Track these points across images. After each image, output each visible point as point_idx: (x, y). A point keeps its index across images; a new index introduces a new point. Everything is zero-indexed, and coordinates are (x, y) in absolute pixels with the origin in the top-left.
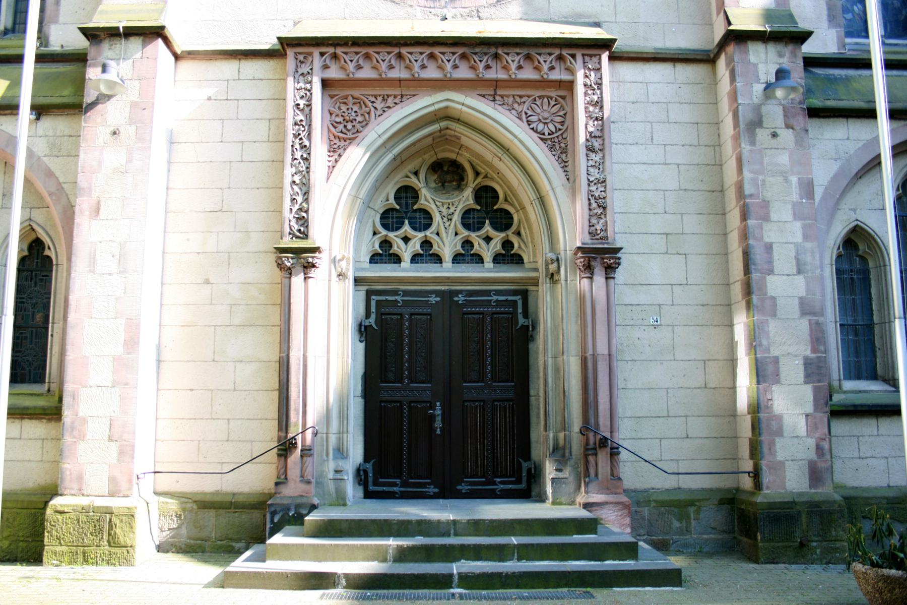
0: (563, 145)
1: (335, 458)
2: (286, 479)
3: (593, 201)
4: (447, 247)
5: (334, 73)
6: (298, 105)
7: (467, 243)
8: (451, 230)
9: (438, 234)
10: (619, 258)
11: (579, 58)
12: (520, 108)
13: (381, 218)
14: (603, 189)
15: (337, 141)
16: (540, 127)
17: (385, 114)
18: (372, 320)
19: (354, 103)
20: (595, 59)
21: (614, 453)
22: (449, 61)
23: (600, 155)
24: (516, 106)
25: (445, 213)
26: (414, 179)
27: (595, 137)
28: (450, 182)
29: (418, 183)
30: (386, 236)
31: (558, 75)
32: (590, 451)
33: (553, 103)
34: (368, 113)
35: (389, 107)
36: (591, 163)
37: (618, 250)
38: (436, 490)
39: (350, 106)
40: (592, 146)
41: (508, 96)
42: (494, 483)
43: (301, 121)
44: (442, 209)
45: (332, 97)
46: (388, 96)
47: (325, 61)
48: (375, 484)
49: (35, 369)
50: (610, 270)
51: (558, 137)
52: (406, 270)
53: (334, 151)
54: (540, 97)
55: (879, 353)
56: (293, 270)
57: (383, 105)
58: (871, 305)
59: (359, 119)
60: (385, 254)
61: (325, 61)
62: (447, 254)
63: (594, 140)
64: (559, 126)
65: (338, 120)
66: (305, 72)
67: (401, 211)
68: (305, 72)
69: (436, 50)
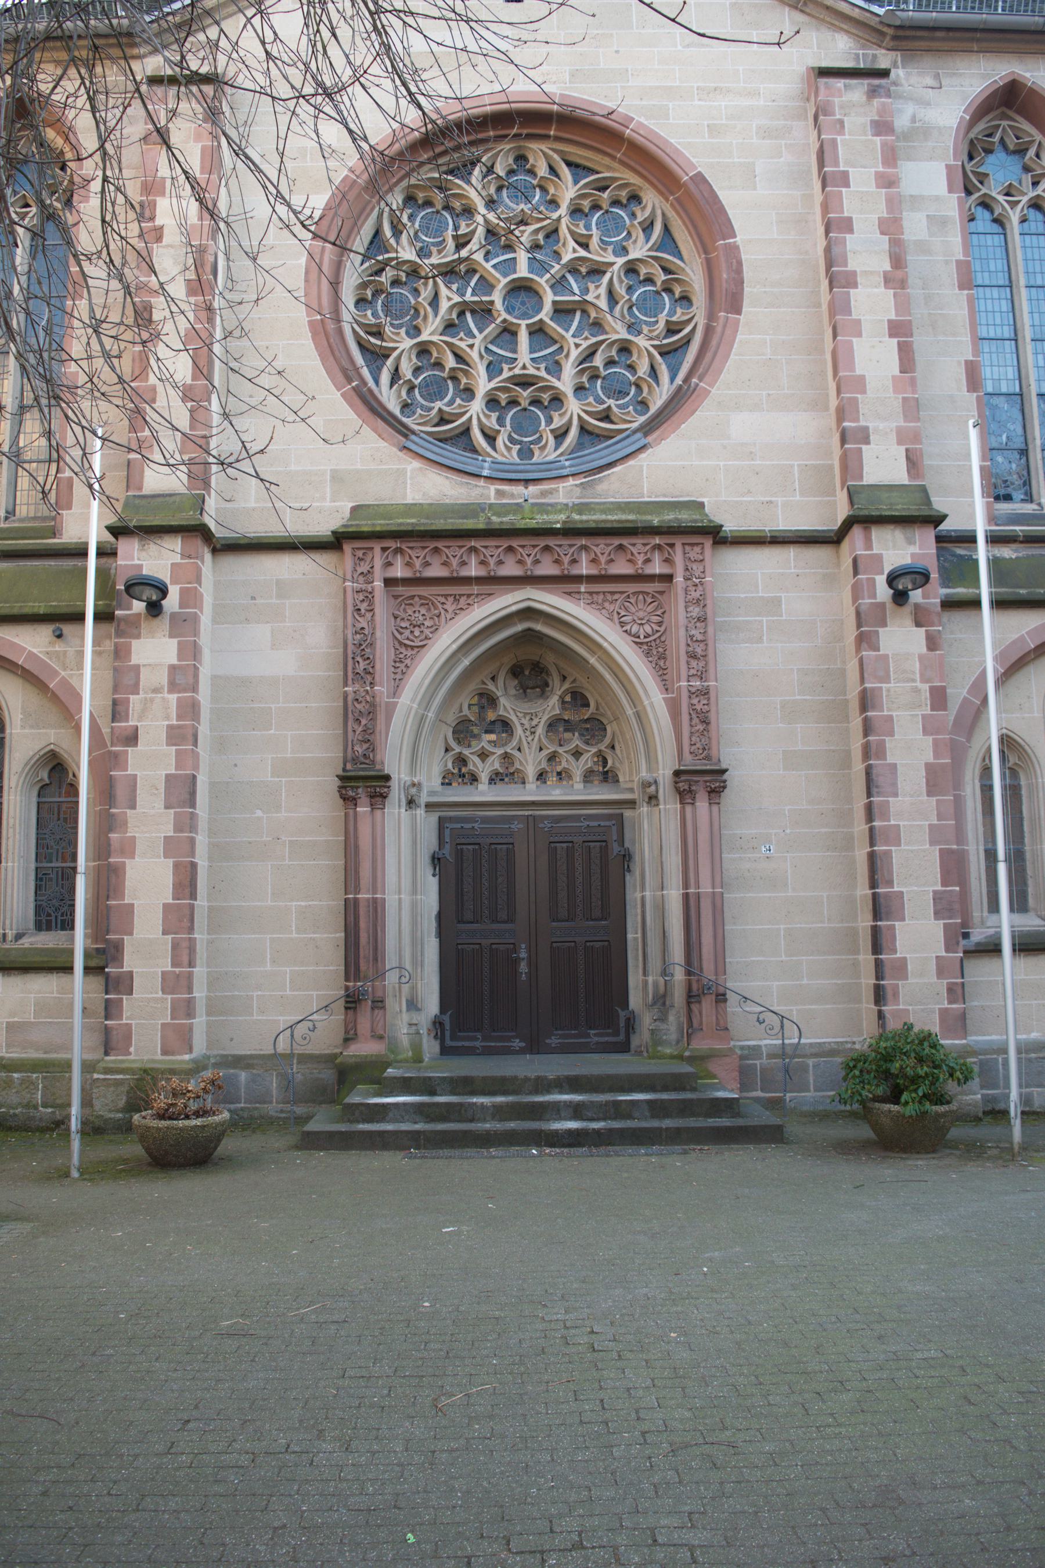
0: (660, 650)
1: (408, 1010)
3: (694, 716)
4: (530, 763)
5: (399, 571)
7: (552, 758)
8: (535, 745)
10: (725, 781)
11: (679, 548)
14: (705, 702)
15: (403, 650)
18: (447, 850)
19: (422, 604)
20: (697, 549)
21: (721, 998)
22: (529, 555)
23: (702, 664)
24: (606, 605)
25: (527, 726)
26: (491, 686)
27: (697, 641)
30: (460, 753)
31: (657, 568)
32: (692, 997)
33: (649, 600)
35: (461, 609)
36: (692, 672)
37: (724, 771)
39: (417, 608)
41: (597, 593)
42: (588, 1036)
44: (523, 721)
45: (396, 597)
46: (461, 595)
47: (387, 557)
49: (62, 915)
50: (716, 792)
51: (655, 640)
52: (484, 792)
53: (401, 662)
54: (634, 593)
55: (1030, 882)
57: (454, 607)
58: (1022, 825)
59: (427, 623)
60: (460, 773)
61: (387, 557)
63: (696, 645)
64: (656, 628)
65: (403, 625)
66: (365, 571)
67: (474, 722)
68: (365, 571)
69: (515, 543)
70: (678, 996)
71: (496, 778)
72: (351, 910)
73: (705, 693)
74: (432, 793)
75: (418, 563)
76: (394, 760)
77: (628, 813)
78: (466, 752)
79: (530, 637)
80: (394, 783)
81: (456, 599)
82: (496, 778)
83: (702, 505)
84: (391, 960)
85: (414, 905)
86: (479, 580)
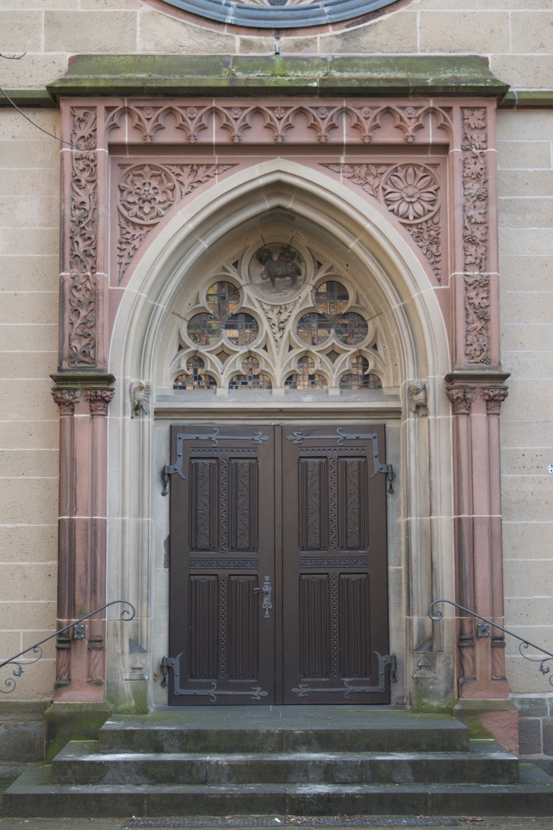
0: (433, 233)
2: (70, 680)
3: (471, 311)
5: (126, 135)
6: (79, 181)
9: (265, 348)
10: (506, 389)
11: (456, 113)
12: (376, 183)
13: (189, 327)
14: (485, 295)
15: (130, 229)
16: (403, 208)
17: (195, 192)
18: (179, 465)
19: (153, 176)
20: (478, 114)
21: (498, 642)
24: (370, 179)
25: (275, 321)
26: (233, 274)
28: (283, 276)
29: (240, 278)
30: (196, 351)
32: (463, 641)
34: (172, 190)
36: (470, 259)
37: (505, 377)
38: (265, 693)
39: (147, 180)
40: (472, 236)
41: (360, 165)
42: (342, 685)
43: (83, 203)
45: (122, 166)
46: (199, 166)
48: (182, 686)
50: (495, 401)
51: (426, 222)
52: (223, 398)
54: (403, 166)
56: (76, 406)
57: (191, 179)
59: (159, 198)
60: (196, 375)
62: (278, 375)
64: (428, 207)
65: (131, 199)
66: (86, 135)
67: (214, 315)
69: (263, 104)
70: (448, 640)
71: (237, 381)
72: (66, 533)
73: (484, 284)
74: (162, 398)
75: (148, 126)
76: (119, 359)
77: (391, 425)
78: (203, 350)
79: (280, 215)
80: (118, 386)
81: (194, 169)
82: (237, 381)
83: (485, 61)
84: (112, 593)
85: (140, 529)
86: (221, 148)
